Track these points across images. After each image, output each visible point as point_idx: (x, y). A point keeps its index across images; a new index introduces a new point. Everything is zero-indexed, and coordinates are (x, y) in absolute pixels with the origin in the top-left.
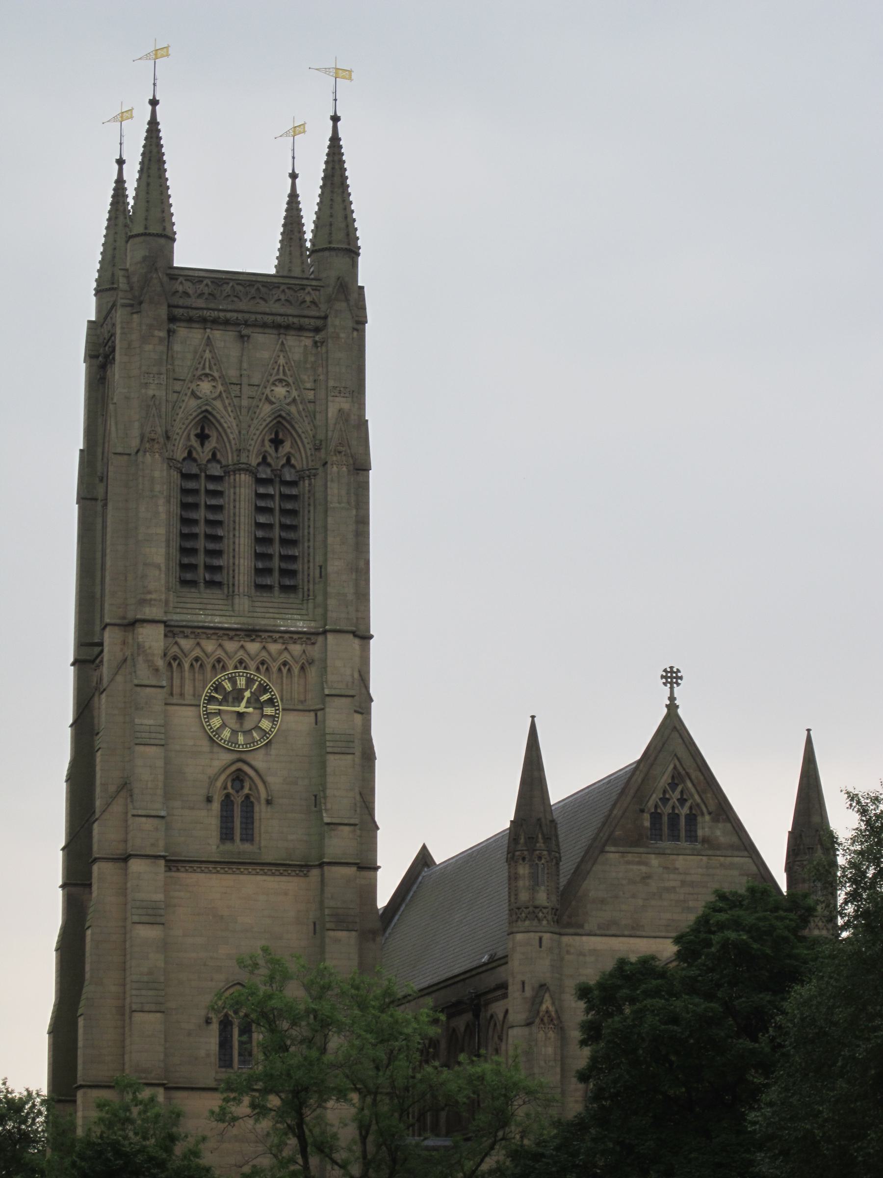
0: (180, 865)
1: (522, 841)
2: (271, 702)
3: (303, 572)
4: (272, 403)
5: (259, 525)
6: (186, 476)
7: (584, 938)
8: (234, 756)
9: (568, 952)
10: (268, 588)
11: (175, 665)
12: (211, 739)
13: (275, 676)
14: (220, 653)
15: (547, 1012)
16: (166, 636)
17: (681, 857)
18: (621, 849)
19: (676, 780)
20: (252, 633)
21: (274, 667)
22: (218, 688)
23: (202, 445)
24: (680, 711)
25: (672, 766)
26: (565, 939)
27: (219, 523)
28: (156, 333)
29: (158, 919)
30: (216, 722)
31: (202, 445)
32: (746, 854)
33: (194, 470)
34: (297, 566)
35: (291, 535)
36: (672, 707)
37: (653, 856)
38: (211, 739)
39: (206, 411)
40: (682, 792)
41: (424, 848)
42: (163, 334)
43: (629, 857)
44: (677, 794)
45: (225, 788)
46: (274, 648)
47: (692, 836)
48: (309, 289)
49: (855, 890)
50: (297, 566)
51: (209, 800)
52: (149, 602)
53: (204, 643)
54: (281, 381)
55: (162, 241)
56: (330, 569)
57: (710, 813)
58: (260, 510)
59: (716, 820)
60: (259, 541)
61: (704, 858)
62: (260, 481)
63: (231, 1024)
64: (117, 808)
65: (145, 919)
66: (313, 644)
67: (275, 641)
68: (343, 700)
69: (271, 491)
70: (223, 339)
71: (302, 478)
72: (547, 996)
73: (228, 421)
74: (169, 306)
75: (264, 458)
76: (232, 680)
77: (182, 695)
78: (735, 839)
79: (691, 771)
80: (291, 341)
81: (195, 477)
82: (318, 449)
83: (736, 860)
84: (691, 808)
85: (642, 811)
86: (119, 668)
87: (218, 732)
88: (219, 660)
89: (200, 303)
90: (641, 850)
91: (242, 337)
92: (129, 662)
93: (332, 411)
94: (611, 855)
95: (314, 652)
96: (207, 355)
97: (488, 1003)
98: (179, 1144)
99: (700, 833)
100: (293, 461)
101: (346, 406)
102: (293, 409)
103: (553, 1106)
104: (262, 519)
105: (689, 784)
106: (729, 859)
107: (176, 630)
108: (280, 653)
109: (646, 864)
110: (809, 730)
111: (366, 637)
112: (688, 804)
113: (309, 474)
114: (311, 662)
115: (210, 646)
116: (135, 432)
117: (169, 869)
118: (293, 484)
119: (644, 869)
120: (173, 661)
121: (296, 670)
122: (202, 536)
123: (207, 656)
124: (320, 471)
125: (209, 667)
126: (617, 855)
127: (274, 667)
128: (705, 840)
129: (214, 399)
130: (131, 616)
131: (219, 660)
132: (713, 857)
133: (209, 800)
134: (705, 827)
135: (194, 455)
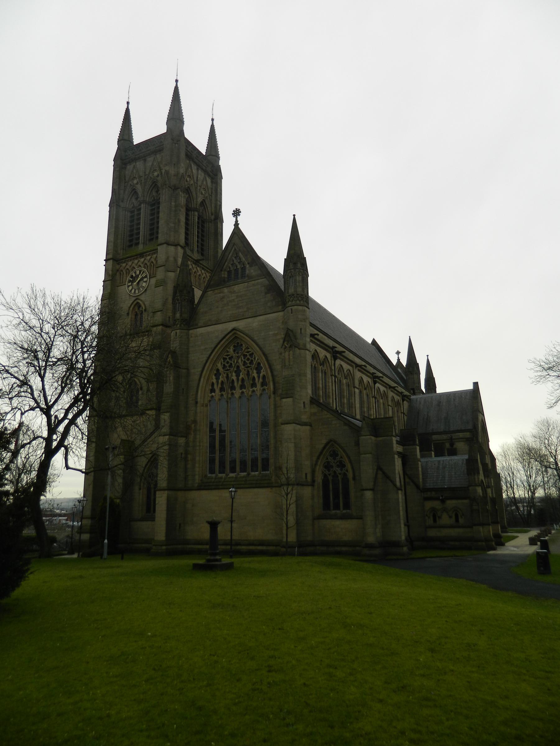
3: (191, 225)
7: (198, 330)
8: (134, 298)
9: (191, 337)
17: (236, 286)
18: (213, 289)
24: (239, 226)
26: (191, 332)
32: (264, 277)
37: (225, 288)
41: (374, 339)
43: (216, 291)
47: (243, 276)
61: (246, 284)
83: (259, 281)
94: (209, 292)
103: (23, 373)
106: (256, 281)
110: (294, 215)
119: (221, 295)
126: (211, 292)
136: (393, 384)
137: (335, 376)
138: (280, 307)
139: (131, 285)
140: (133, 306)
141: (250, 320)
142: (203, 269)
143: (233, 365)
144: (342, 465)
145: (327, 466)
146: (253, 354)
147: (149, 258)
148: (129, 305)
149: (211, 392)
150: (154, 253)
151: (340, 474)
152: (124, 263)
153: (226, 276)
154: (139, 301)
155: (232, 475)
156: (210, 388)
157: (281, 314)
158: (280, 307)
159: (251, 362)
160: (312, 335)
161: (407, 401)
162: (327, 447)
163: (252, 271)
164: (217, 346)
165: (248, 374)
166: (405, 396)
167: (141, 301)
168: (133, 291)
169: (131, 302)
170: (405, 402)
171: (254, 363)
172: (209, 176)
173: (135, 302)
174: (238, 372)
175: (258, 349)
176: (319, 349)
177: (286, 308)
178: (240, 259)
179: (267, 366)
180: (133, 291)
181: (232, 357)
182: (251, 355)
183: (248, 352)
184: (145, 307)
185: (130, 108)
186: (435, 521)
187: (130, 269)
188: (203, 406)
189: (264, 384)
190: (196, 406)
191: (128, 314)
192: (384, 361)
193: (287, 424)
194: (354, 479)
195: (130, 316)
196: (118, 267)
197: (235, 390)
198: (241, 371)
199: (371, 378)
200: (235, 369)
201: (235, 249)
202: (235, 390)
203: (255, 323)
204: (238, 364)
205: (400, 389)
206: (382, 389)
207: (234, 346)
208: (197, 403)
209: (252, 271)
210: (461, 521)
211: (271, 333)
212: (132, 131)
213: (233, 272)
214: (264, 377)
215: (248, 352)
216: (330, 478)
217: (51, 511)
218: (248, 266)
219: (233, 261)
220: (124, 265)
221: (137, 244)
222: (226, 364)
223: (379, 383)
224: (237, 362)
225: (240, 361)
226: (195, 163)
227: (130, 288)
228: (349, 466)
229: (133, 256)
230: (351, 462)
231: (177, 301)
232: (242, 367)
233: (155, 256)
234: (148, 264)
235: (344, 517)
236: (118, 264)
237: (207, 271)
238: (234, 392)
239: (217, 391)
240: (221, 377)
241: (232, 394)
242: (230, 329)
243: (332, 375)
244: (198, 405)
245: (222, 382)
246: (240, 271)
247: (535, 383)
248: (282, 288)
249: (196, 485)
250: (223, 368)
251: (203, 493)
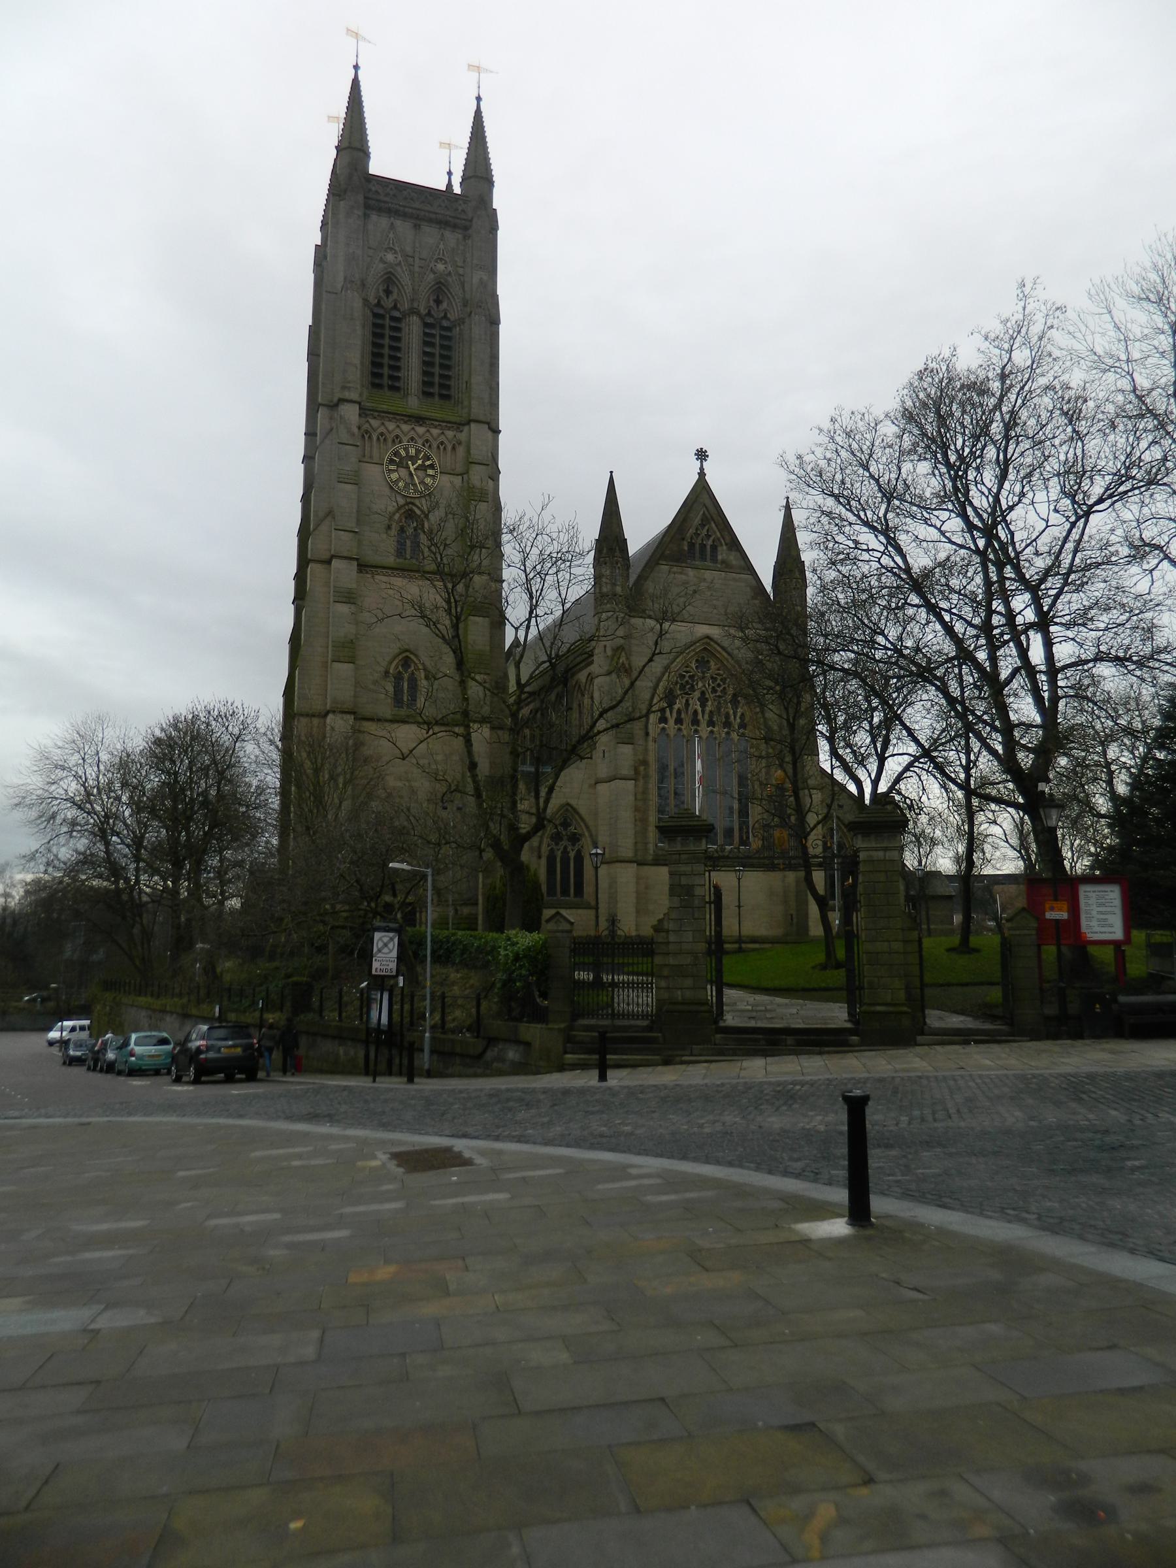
0: (368, 569)
1: (605, 551)
2: (432, 467)
4: (435, 273)
5: (425, 353)
6: (375, 315)
10: (431, 395)
11: (366, 437)
12: (391, 488)
13: (435, 450)
14: (398, 432)
15: (623, 664)
16: (360, 415)
19: (705, 521)
20: (419, 420)
21: (435, 445)
22: (396, 454)
23: (388, 297)
28: (356, 212)
29: (352, 601)
30: (394, 476)
31: (388, 297)
33: (381, 311)
34: (452, 383)
35: (447, 362)
36: (702, 474)
38: (391, 488)
39: (390, 272)
40: (708, 531)
42: (360, 213)
43: (675, 569)
44: (705, 532)
45: (401, 521)
46: (435, 432)
47: (714, 559)
48: (461, 202)
49: (433, 869)
50: (452, 383)
51: (389, 527)
52: (349, 388)
53: (387, 423)
54: (441, 259)
55: (361, 154)
56: (473, 381)
57: (726, 544)
58: (426, 343)
59: (730, 549)
60: (425, 363)
62: (426, 325)
63: (402, 679)
64: (324, 528)
65: (344, 600)
66: (461, 431)
67: (436, 427)
68: (482, 467)
69: (433, 332)
70: (403, 227)
71: (455, 326)
72: (623, 654)
73: (405, 278)
74: (365, 198)
75: (429, 311)
76: (406, 450)
77: (371, 457)
78: (742, 563)
79: (714, 516)
80: (448, 234)
81: (382, 317)
82: (465, 305)
84: (713, 541)
85: (683, 539)
86: (328, 434)
87: (396, 482)
88: (397, 436)
89: (387, 199)
90: (683, 565)
91: (417, 227)
92: (334, 430)
93: (475, 280)
95: (463, 436)
96: (391, 235)
97: (573, 675)
99: (720, 557)
100: (449, 315)
101: (485, 278)
102: (449, 279)
104: (428, 350)
105: (713, 525)
107: (369, 412)
108: (439, 435)
109: (685, 574)
110: (611, 472)
111: (497, 432)
112: (712, 539)
113: (461, 321)
114: (460, 443)
115: (391, 426)
116: (341, 278)
117: (360, 571)
118: (448, 329)
119: (684, 577)
120: (365, 434)
121: (449, 447)
122: (387, 336)
123: (389, 432)
124: (467, 320)
125: (390, 441)
127: (435, 445)
128: (723, 562)
129: (396, 265)
130: (338, 395)
131: (397, 436)
133: (389, 527)
134: (723, 553)
135: (382, 302)
173: (404, 655)
185: (482, 109)
190: (646, 741)
207: (697, 661)
208: (647, 734)
212: (367, 135)
217: (710, 943)
229: (398, 415)
244: (650, 738)
249: (650, 858)
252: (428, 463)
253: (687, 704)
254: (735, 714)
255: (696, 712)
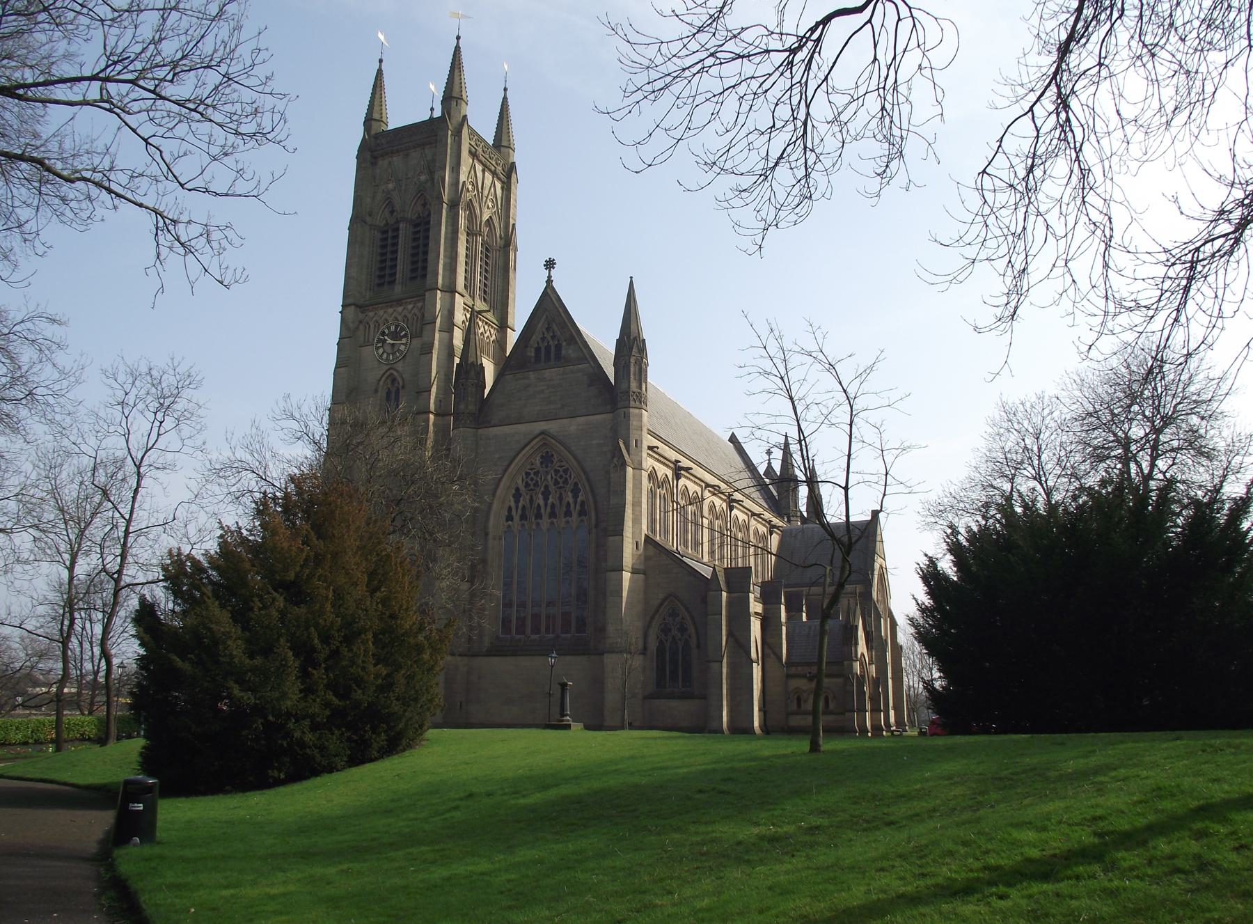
7: (491, 429)
8: (388, 367)
25: (544, 317)
26: (480, 431)
27: (414, 248)
36: (549, 281)
47: (558, 356)
94: (508, 377)
98: (207, 546)
108: (412, 309)
119: (526, 381)
132: (1169, 343)
133: (376, 391)
136: (757, 510)
137: (677, 503)
138: (609, 407)
139: (382, 347)
140: (383, 379)
141: (565, 420)
142: (486, 323)
143: (540, 483)
144: (683, 629)
145: (665, 630)
146: (568, 469)
147: (410, 307)
148: (378, 377)
149: (507, 521)
150: (419, 301)
151: (680, 640)
152: (371, 311)
153: (533, 354)
154: (395, 373)
155: (536, 637)
156: (506, 513)
157: (609, 416)
158: (609, 407)
159: (566, 482)
160: (650, 448)
161: (776, 533)
162: (666, 603)
163: (569, 352)
164: (518, 455)
165: (561, 499)
166: (775, 527)
167: (397, 371)
168: (385, 356)
169: (382, 372)
170: (774, 535)
171: (570, 482)
172: (499, 179)
173: (388, 373)
174: (546, 495)
175: (575, 463)
176: (658, 466)
177: (617, 409)
178: (554, 332)
179: (588, 489)
180: (385, 356)
181: (538, 472)
182: (566, 471)
183: (561, 467)
184: (403, 381)
186: (799, 705)
187: (380, 321)
188: (494, 539)
189: (582, 513)
191: (376, 391)
192: (681, 771)
193: (614, 571)
194: (698, 646)
195: (379, 394)
196: (361, 316)
197: (541, 519)
198: (550, 493)
199: (725, 501)
200: (542, 489)
201: (547, 317)
202: (541, 519)
203: (571, 426)
204: (545, 482)
205: (767, 516)
206: (742, 517)
207: (542, 457)
208: (487, 534)
209: (570, 351)
210: (832, 706)
211: (594, 442)
213: (543, 349)
214: (583, 503)
215: (561, 467)
216: (668, 645)
218: (564, 343)
219: (544, 334)
220: (371, 314)
221: (392, 282)
222: (530, 482)
223: (737, 508)
224: (545, 479)
225: (549, 477)
226: (480, 161)
227: (381, 351)
228: (692, 630)
230: (694, 623)
231: (461, 386)
232: (552, 488)
233: (420, 305)
234: (409, 316)
235: (683, 696)
236: (362, 312)
237: (492, 327)
238: (540, 521)
239: (517, 518)
240: (522, 499)
241: (538, 524)
242: (537, 432)
243: (673, 502)
244: (490, 536)
245: (524, 507)
246: (553, 349)
247: (920, 530)
248: (610, 371)
250: (526, 487)
251: (495, 660)
252: (387, 332)
253: (531, 500)
254: (517, 507)
255: (568, 504)
